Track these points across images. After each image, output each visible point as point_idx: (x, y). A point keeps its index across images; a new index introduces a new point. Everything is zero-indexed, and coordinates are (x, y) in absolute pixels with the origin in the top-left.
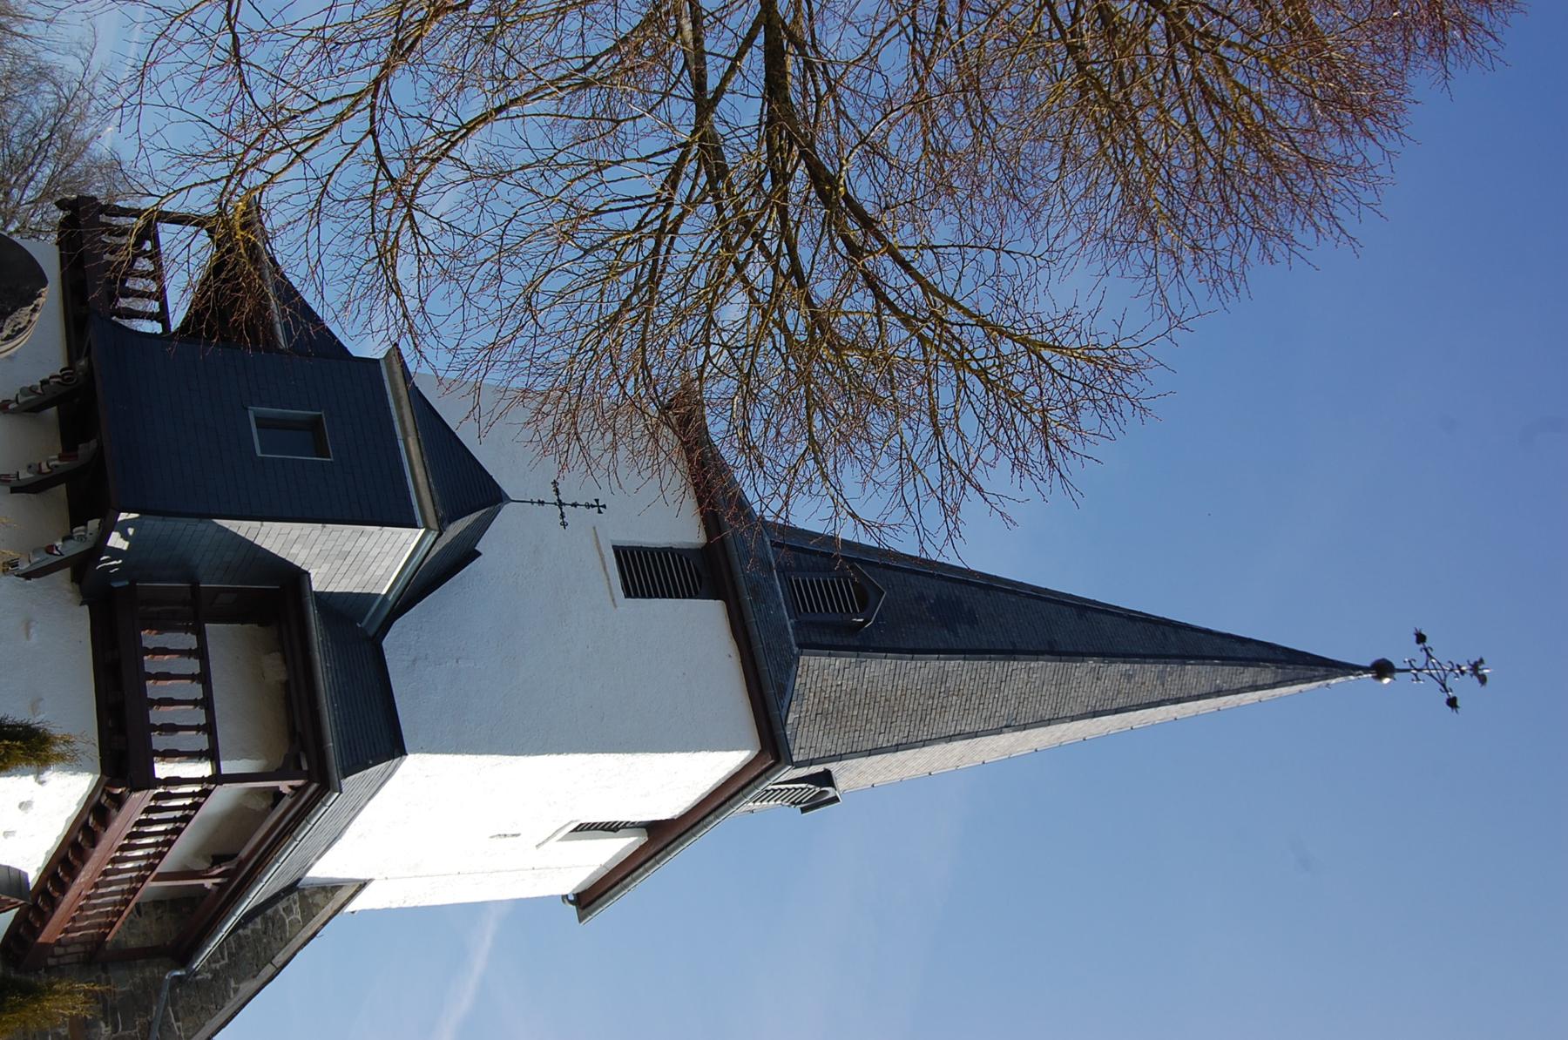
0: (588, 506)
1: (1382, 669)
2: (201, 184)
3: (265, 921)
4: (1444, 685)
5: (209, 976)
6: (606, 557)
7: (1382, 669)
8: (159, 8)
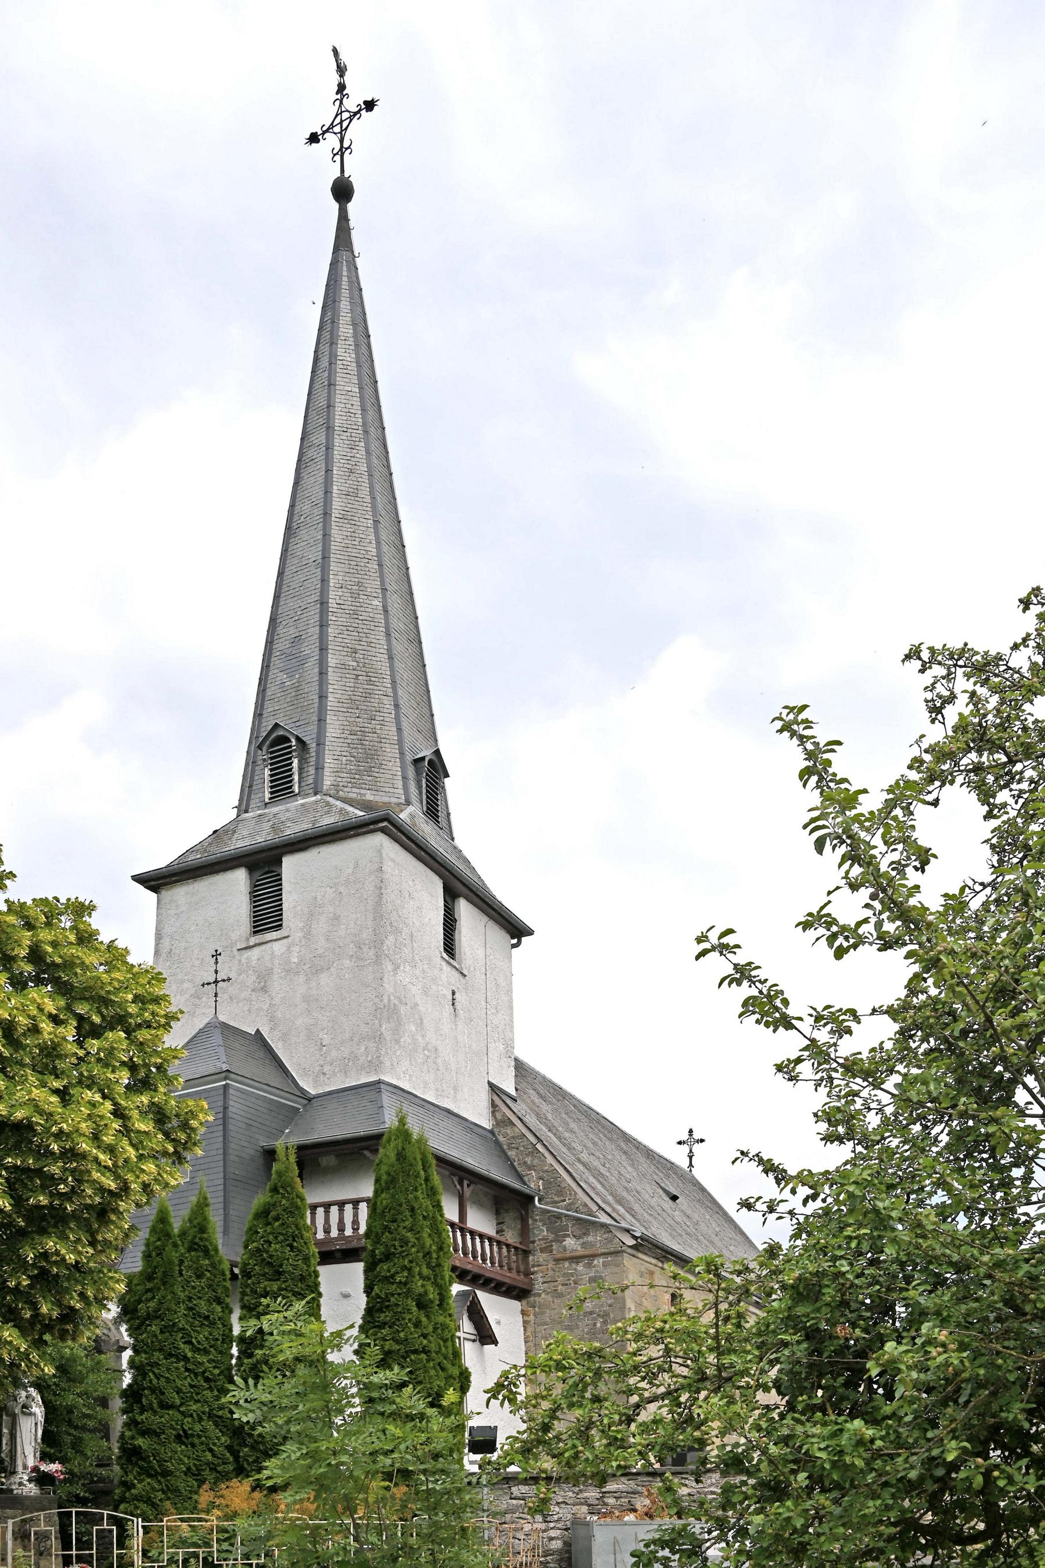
0: (217, 962)
1: (342, 191)
2: (341, 88)
3: (510, 1148)
4: (355, 114)
5: (541, 1182)
6: (257, 942)
7: (342, 191)
8: (341, 70)
